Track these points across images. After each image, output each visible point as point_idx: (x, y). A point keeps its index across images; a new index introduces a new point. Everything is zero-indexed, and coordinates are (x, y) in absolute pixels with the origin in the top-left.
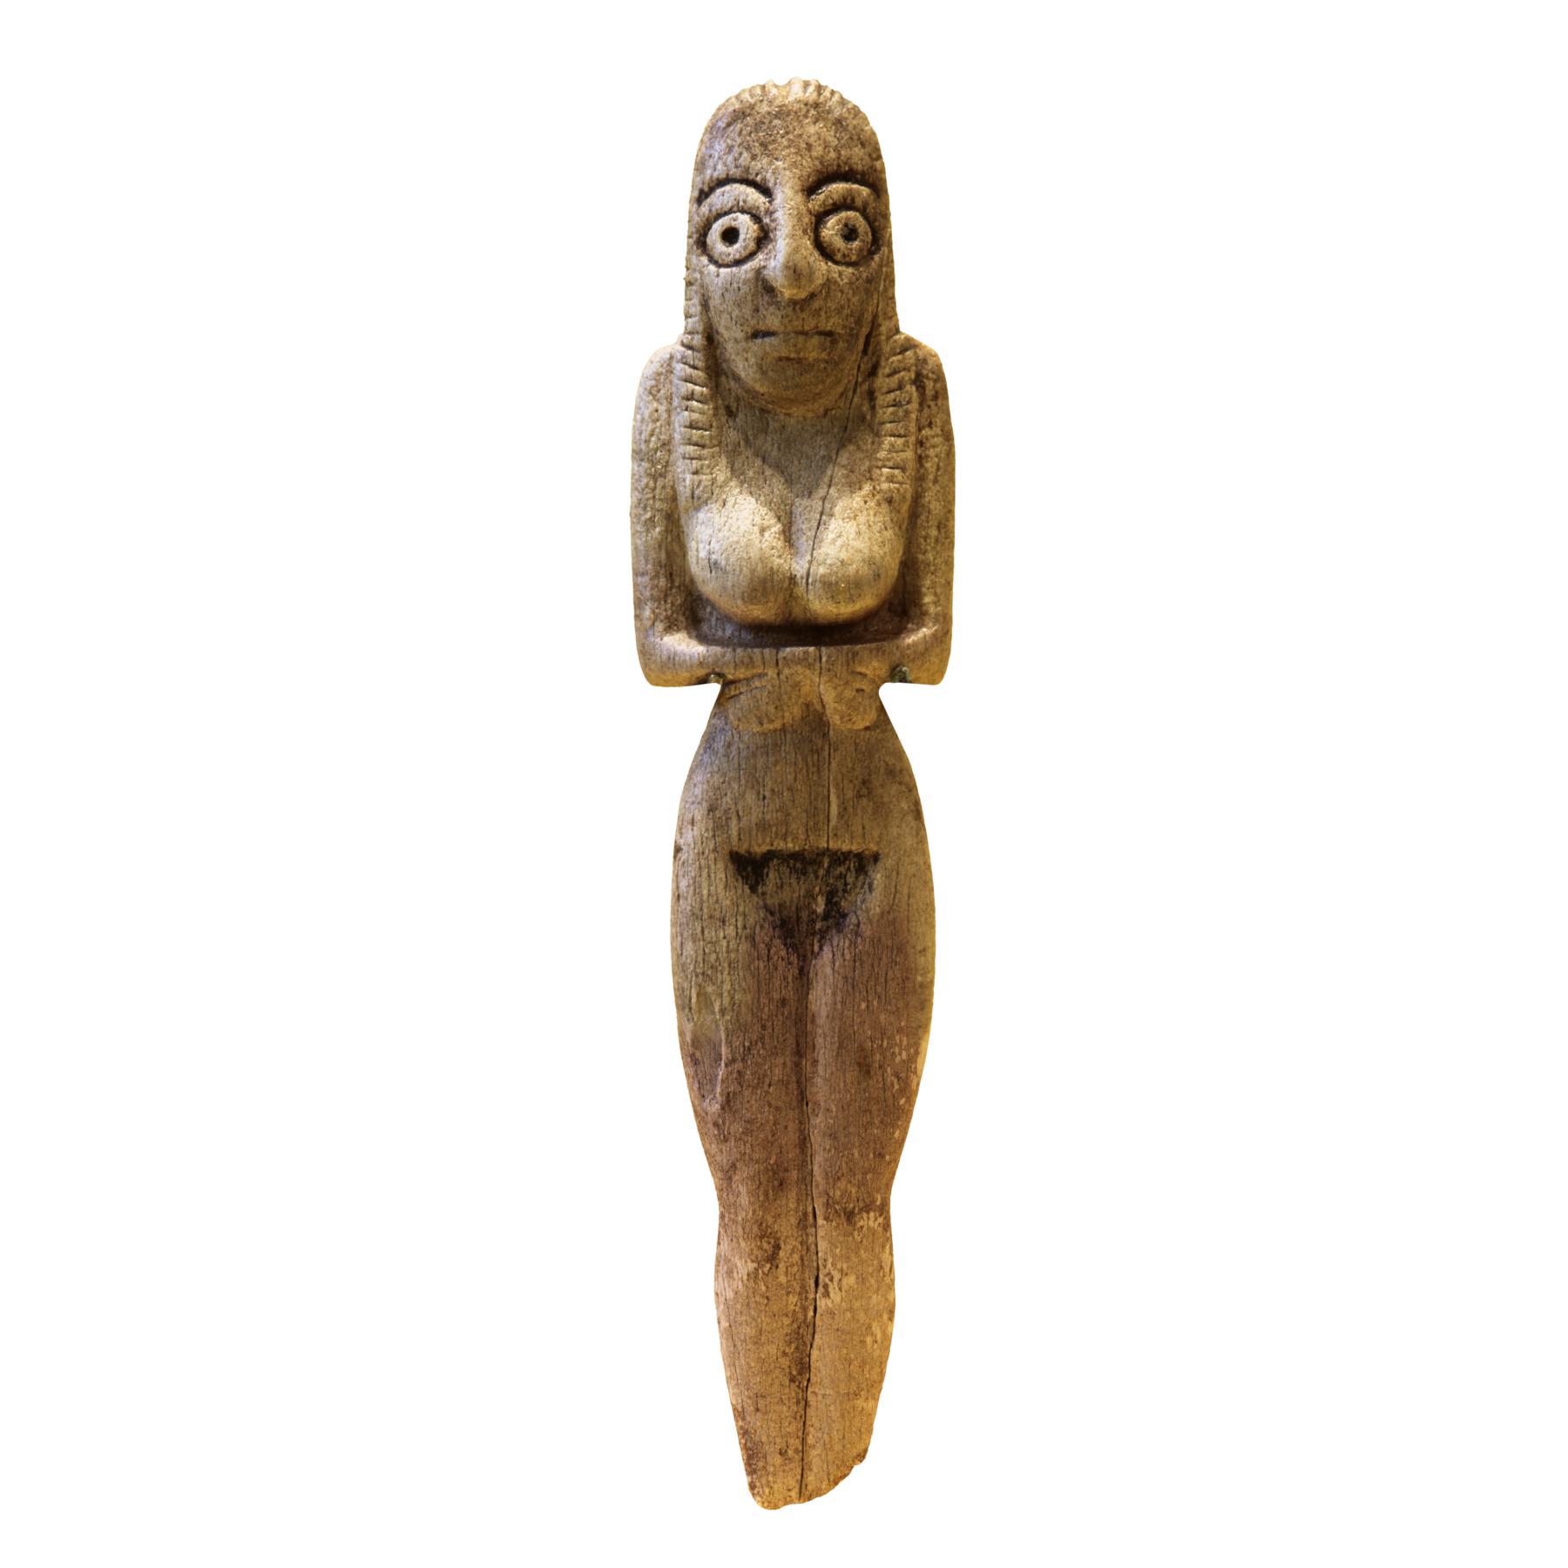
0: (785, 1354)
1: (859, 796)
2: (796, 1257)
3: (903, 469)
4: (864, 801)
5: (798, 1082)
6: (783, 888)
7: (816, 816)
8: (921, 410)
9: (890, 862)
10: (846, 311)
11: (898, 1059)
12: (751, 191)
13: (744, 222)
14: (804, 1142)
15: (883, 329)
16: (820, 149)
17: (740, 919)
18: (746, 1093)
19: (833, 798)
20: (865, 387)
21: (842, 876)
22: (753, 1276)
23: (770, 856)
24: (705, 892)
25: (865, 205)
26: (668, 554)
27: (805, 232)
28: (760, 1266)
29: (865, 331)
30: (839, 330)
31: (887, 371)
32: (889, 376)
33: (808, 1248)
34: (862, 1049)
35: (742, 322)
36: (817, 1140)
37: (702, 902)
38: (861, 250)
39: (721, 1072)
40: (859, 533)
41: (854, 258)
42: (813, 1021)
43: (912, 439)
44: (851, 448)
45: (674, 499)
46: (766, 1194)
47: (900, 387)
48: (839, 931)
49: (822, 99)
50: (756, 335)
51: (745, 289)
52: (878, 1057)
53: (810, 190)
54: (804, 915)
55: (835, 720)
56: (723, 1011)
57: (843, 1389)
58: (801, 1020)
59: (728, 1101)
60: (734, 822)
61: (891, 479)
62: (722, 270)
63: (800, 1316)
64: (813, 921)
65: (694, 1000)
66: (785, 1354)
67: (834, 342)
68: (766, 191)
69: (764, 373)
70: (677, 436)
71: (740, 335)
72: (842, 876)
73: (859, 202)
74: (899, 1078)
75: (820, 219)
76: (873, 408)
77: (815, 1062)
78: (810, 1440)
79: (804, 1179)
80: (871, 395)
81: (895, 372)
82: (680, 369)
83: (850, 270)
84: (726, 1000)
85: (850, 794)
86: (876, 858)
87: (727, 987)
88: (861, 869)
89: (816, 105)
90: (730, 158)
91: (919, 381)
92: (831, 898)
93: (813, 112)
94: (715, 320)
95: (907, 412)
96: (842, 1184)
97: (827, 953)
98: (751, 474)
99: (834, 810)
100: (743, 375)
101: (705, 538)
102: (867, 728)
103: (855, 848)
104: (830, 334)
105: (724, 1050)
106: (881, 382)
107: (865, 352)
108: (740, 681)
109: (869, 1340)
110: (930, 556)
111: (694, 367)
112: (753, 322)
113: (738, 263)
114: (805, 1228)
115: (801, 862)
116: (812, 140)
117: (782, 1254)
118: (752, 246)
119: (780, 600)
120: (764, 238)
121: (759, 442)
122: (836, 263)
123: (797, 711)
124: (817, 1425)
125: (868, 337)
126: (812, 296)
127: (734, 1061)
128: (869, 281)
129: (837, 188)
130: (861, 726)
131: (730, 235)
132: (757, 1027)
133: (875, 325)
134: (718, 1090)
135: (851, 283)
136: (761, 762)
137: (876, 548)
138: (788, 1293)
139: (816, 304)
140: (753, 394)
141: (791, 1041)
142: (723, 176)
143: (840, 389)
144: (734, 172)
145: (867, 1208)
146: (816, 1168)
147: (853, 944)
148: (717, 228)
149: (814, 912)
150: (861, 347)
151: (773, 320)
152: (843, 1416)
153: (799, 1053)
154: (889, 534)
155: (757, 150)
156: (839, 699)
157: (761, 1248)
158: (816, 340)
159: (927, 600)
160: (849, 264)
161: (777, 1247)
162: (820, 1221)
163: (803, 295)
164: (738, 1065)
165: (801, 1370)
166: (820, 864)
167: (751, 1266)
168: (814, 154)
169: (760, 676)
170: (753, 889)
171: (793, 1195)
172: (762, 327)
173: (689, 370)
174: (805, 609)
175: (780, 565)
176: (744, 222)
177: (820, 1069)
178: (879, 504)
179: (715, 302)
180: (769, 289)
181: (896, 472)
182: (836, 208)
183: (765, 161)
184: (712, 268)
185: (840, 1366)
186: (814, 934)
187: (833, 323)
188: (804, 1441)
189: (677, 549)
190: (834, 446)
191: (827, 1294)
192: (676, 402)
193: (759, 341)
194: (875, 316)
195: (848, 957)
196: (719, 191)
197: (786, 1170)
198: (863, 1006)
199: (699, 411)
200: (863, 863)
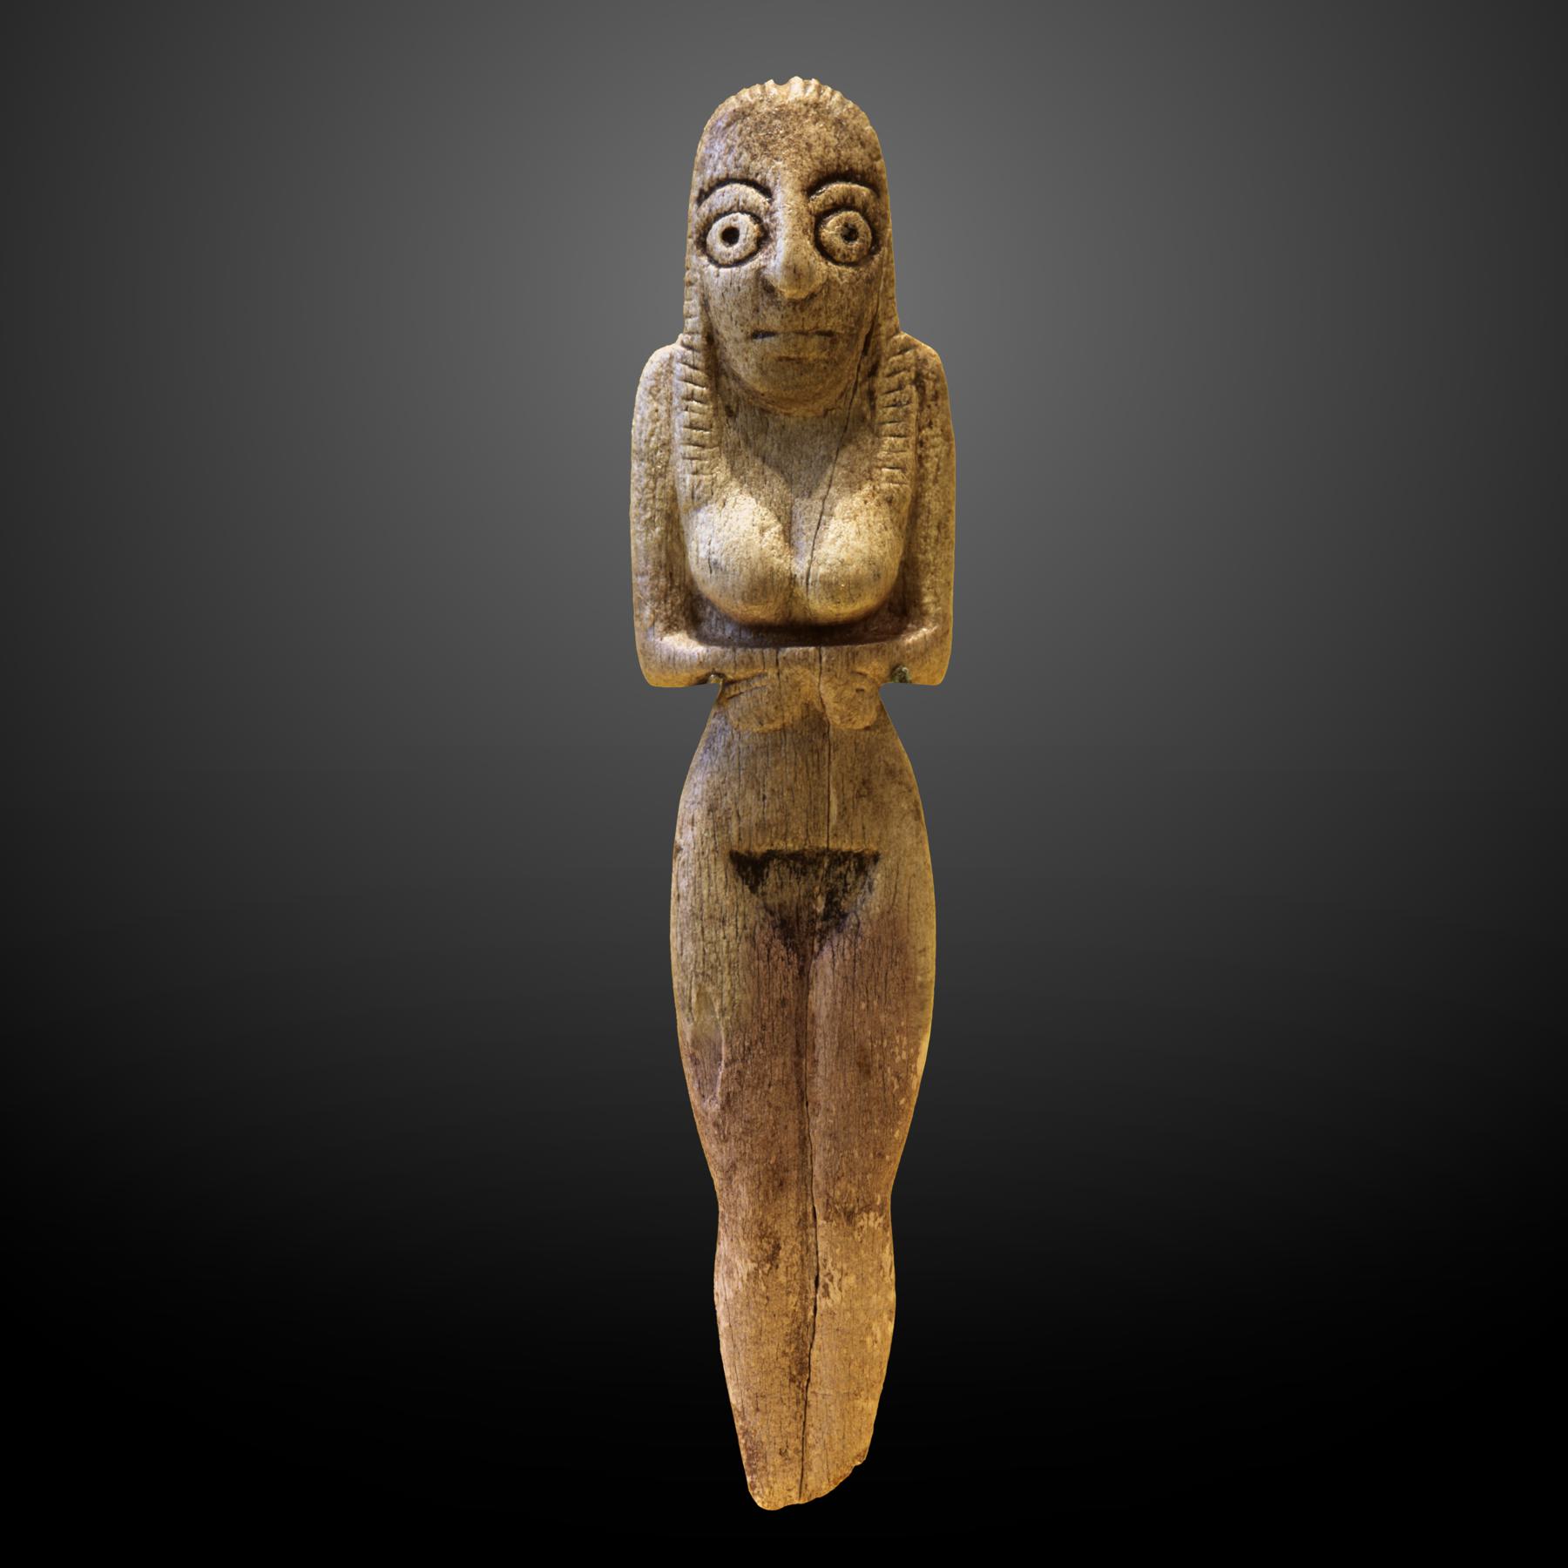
0: (785, 1354)
1: (859, 796)
2: (796, 1257)
3: (903, 469)
4: (864, 801)
5: (798, 1082)
6: (783, 888)
7: (816, 816)
8: (921, 410)
9: (890, 862)
10: (846, 311)
11: (898, 1059)
12: (751, 191)
13: (744, 222)
14: (804, 1142)
15: (883, 329)
16: (820, 149)
17: (740, 919)
18: (746, 1093)
19: (833, 798)
20: (865, 387)
21: (842, 876)
22: (753, 1276)
23: (770, 856)
24: (705, 892)
25: (865, 205)
26: (668, 554)
27: (805, 232)
28: (760, 1266)
29: (865, 331)
30: (839, 330)
31: (887, 371)
32: (889, 376)
33: (808, 1248)
34: (862, 1049)
35: (742, 322)
36: (817, 1140)
37: (702, 902)
38: (861, 250)
39: (721, 1072)
40: (859, 533)
41: (854, 258)
42: (813, 1021)
43: (912, 439)
44: (851, 448)
45: (674, 499)
46: (766, 1194)
47: (900, 387)
48: (839, 931)
49: (822, 99)
50: (756, 335)
51: (745, 289)
52: (878, 1057)
53: (810, 190)
54: (804, 915)
55: (835, 720)
56: (723, 1011)
57: (843, 1389)
58: (801, 1020)
59: (728, 1101)
60: (734, 822)
61: (891, 479)
62: (722, 270)
63: (800, 1316)
64: (813, 921)
65: (694, 1000)
66: (785, 1354)
67: (834, 342)
68: (766, 191)
69: (764, 373)
70: (677, 436)
71: (740, 335)
72: (842, 876)
73: (859, 202)
74: (899, 1078)
75: (820, 219)
76: (873, 408)
77: (815, 1062)
78: (810, 1440)
79: (804, 1179)
80: (871, 395)
81: (895, 372)
82: (680, 369)
83: (850, 270)
84: (726, 1000)
85: (850, 794)
86: (876, 858)
87: (727, 987)
88: (861, 869)
89: (816, 105)
90: (730, 158)
91: (918, 381)
92: (831, 898)
93: (813, 112)
94: (715, 320)
95: (907, 412)
96: (842, 1184)
97: (827, 953)
98: (751, 474)
99: (834, 810)
100: (743, 375)
101: (705, 538)
102: (867, 728)
103: (855, 848)
104: (830, 334)
105: (724, 1050)
106: (881, 382)
107: (865, 352)
108: (740, 681)
109: (869, 1340)
110: (930, 556)
111: (694, 367)
112: (753, 322)
113: (738, 263)
114: (805, 1228)
115: (801, 862)
116: (812, 140)
117: (782, 1254)
118: (752, 246)
119: (780, 600)
120: (764, 238)
121: (759, 442)
122: (836, 263)
123: (797, 711)
124: (817, 1425)
125: (868, 337)
126: (812, 296)
127: (734, 1061)
128: (869, 281)
129: (837, 188)
130: (861, 726)
131: (730, 235)
132: (757, 1027)
133: (875, 325)
134: (718, 1090)
135: (851, 283)
136: (761, 762)
137: (876, 548)
138: (788, 1293)
139: (816, 304)
140: (753, 394)
141: (791, 1041)
142: (723, 176)
143: (840, 389)
144: (734, 172)
145: (867, 1208)
146: (816, 1168)
147: (853, 944)
148: (717, 228)
149: (814, 912)
150: (861, 347)
151: (773, 320)
152: (843, 1416)
153: (799, 1053)
154: (889, 534)
155: (757, 150)
156: (839, 699)
157: (761, 1248)
158: (816, 340)
159: (927, 600)
160: (849, 264)
161: (777, 1247)
162: (820, 1221)
163: (803, 295)
164: (738, 1065)
165: (801, 1370)
166: (820, 864)
167: (751, 1266)
168: (814, 154)
169: (760, 676)
170: (753, 889)
171: (793, 1195)
172: (762, 327)
173: (689, 370)
174: (805, 609)
175: (780, 565)
176: (744, 222)
177: (820, 1069)
178: (879, 504)
179: (715, 302)
180: (769, 289)
181: (896, 472)
182: (836, 208)
183: (765, 161)
184: (712, 268)
185: (840, 1366)
186: (814, 934)
187: (833, 323)
188: (804, 1441)
189: (677, 549)
190: (834, 446)
191: (827, 1294)
192: (676, 402)
193: (759, 341)
194: (875, 316)
195: (848, 957)
196: (719, 191)
197: (786, 1170)
198: (863, 1006)
199: (699, 411)
200: (863, 863)
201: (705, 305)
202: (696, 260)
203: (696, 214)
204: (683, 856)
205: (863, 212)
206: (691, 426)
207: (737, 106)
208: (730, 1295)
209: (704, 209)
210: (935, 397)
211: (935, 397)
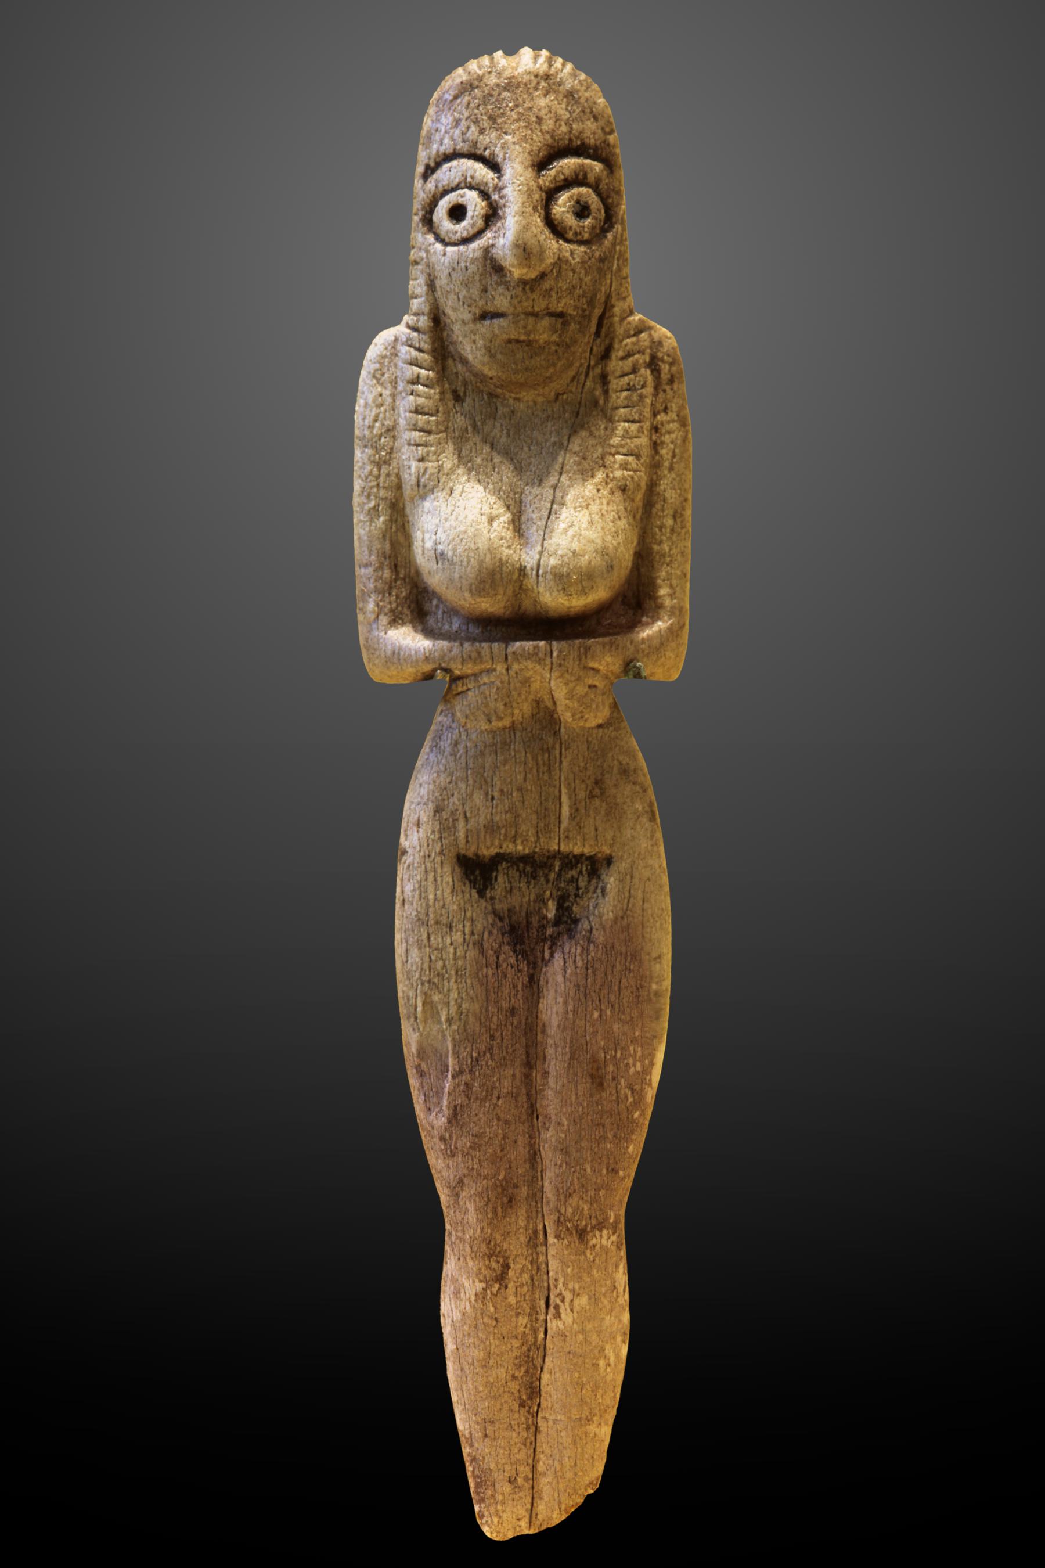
0: (514, 1377)
1: (592, 796)
2: (526, 1277)
3: (638, 456)
4: (597, 802)
6: (512, 892)
7: (547, 817)
8: (656, 395)
9: (622, 864)
10: (578, 292)
11: (632, 1070)
13: (471, 199)
14: (534, 1156)
15: (617, 310)
16: (551, 122)
17: (468, 924)
18: (474, 1106)
19: (565, 799)
21: (574, 880)
22: (481, 1296)
23: (498, 859)
24: (431, 897)
25: (598, 181)
27: (535, 209)
28: (489, 1286)
29: (597, 312)
31: (621, 354)
32: (623, 358)
33: (539, 1269)
34: (594, 1060)
35: (469, 303)
36: (548, 1155)
37: (428, 906)
38: (593, 228)
40: (591, 523)
41: (586, 236)
42: (544, 1032)
43: (647, 425)
44: (584, 433)
45: (399, 487)
47: (634, 370)
49: (553, 71)
50: (484, 316)
52: (611, 1068)
53: (541, 165)
54: (534, 920)
55: (567, 717)
58: (531, 1030)
60: (461, 824)
61: (624, 466)
62: (449, 249)
63: (531, 1339)
64: (544, 927)
65: (419, 1009)
66: (514, 1377)
67: (565, 324)
68: (495, 167)
69: (492, 356)
70: (402, 422)
71: (467, 316)
72: (574, 880)
73: (591, 178)
74: (633, 1091)
75: (550, 195)
76: (606, 392)
77: (546, 1074)
78: (541, 1467)
80: (604, 379)
81: (629, 355)
82: (404, 350)
83: (583, 248)
84: (453, 1010)
85: (582, 795)
86: (609, 861)
87: (454, 995)
89: (547, 77)
93: (543, 84)
94: (442, 301)
95: (641, 397)
96: (574, 1201)
97: (558, 960)
98: (479, 461)
99: (566, 811)
100: (470, 358)
102: (600, 726)
103: (587, 851)
104: (561, 315)
106: (615, 365)
107: (598, 333)
109: (602, 1363)
110: (666, 547)
111: (420, 350)
112: (481, 303)
113: (466, 241)
114: (535, 1246)
115: (532, 865)
116: (542, 113)
117: (511, 1273)
118: (480, 223)
119: (510, 592)
120: (492, 216)
122: (568, 241)
124: (548, 1451)
125: (601, 319)
126: (543, 275)
128: (602, 260)
129: (569, 163)
131: (457, 213)
132: (485, 1037)
133: (608, 306)
134: (445, 1102)
135: (583, 262)
136: (489, 761)
137: (609, 538)
138: (518, 1315)
139: (547, 285)
140: (481, 378)
141: (521, 1051)
142: (450, 151)
146: (546, 1184)
147: (585, 950)
149: (545, 917)
150: (593, 329)
151: (501, 301)
152: (574, 1442)
153: (529, 1064)
154: (622, 524)
157: (489, 1267)
158: (546, 322)
160: (581, 243)
161: (506, 1267)
162: (551, 1240)
163: (533, 275)
164: (466, 1077)
166: (551, 867)
167: (480, 1286)
168: (545, 127)
169: (489, 671)
170: (481, 894)
171: (522, 1212)
172: (490, 308)
173: (414, 353)
174: (535, 602)
176: (471, 199)
178: (612, 493)
179: (441, 282)
180: (498, 269)
181: (630, 459)
182: (567, 184)
183: (494, 135)
184: (439, 246)
186: (544, 940)
189: (401, 539)
190: (566, 432)
191: (558, 1316)
193: (487, 322)
194: (608, 297)
195: (580, 964)
197: (516, 1186)
198: (596, 1015)
199: (425, 395)
201: (431, 285)
202: (422, 238)
203: (422, 190)
204: (408, 859)
205: (596, 189)
206: (417, 411)
207: (465, 78)
208: (457, 1316)
209: (431, 185)
210: (671, 381)
211: (671, 381)
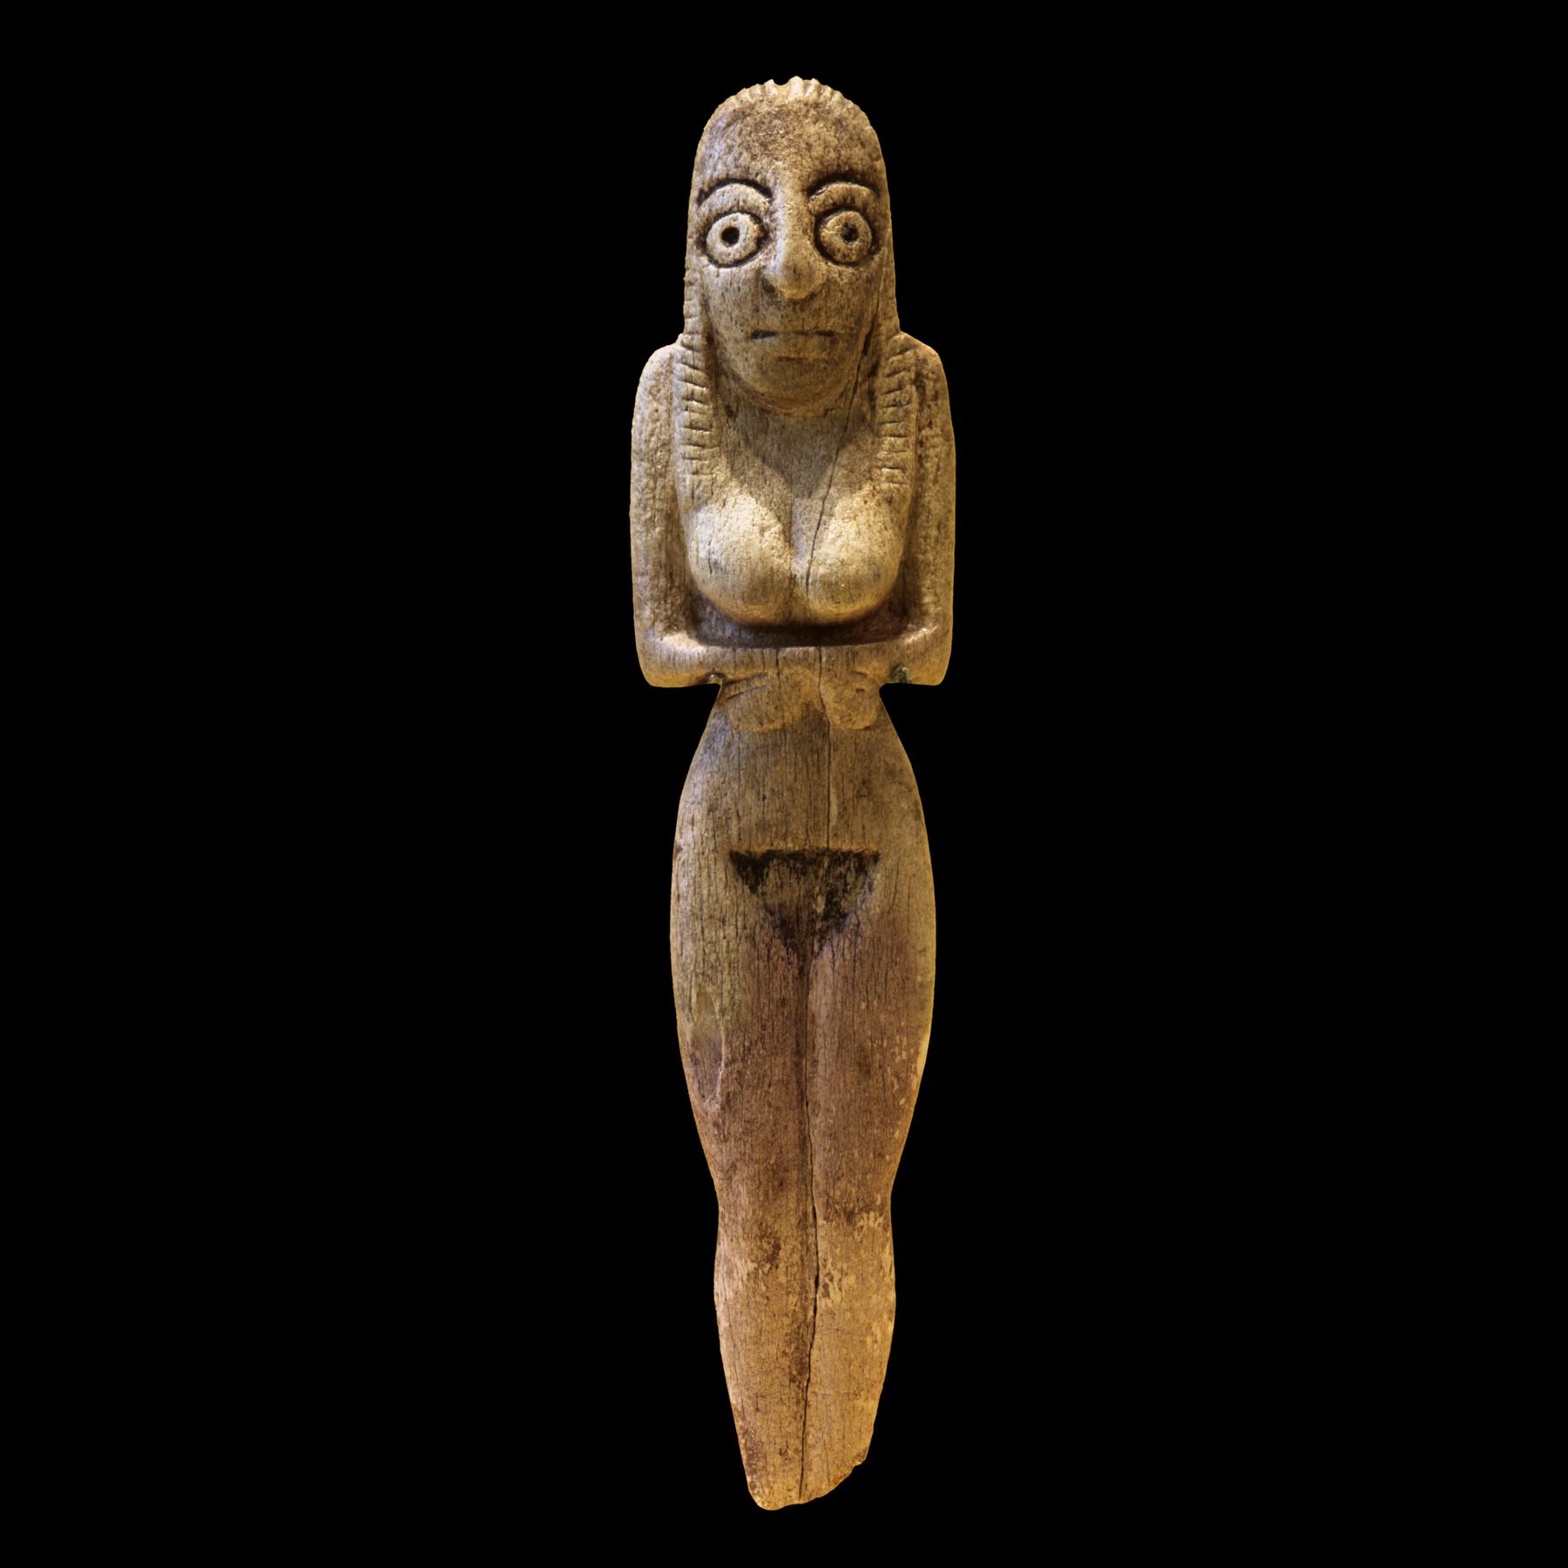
0: (785, 1354)
1: (859, 796)
2: (796, 1257)
3: (903, 469)
4: (864, 801)
5: (798, 1082)
6: (783, 888)
8: (921, 410)
9: (890, 862)
10: (846, 311)
11: (898, 1059)
12: (751, 191)
13: (744, 222)
14: (804, 1142)
15: (883, 329)
16: (820, 149)
17: (740, 919)
18: (746, 1093)
19: (833, 798)
20: (865, 387)
21: (842, 876)
22: (753, 1276)
23: (770, 856)
24: (705, 892)
25: (865, 205)
26: (668, 554)
27: (805, 232)
28: (760, 1266)
29: (865, 331)
30: (839, 330)
31: (887, 371)
32: (889, 376)
33: (808, 1248)
34: (862, 1049)
35: (742, 322)
36: (817, 1140)
37: (702, 902)
38: (861, 250)
39: (721, 1072)
40: (859, 533)
41: (854, 258)
42: (813, 1021)
43: (912, 439)
44: (851, 448)
45: (674, 499)
46: (766, 1194)
47: (900, 387)
48: (839, 931)
49: (822, 99)
50: (756, 335)
51: (745, 289)
52: (878, 1057)
53: (810, 190)
54: (804, 915)
55: (835, 720)
56: (723, 1011)
57: (843, 1389)
58: (801, 1020)
59: (728, 1101)
60: (734, 822)
61: (891, 479)
62: (722, 270)
63: (800, 1316)
64: (813, 921)
65: (694, 1000)
66: (785, 1354)
67: (834, 342)
68: (766, 191)
69: (764, 373)
70: (677, 436)
71: (740, 335)
72: (842, 876)
73: (859, 202)
74: (899, 1078)
75: (820, 219)
76: (873, 408)
77: (815, 1062)
78: (810, 1440)
79: (804, 1179)
80: (871, 395)
81: (895, 372)
83: (850, 270)
84: (726, 1000)
85: (850, 794)
86: (876, 858)
87: (727, 987)
88: (861, 869)
89: (816, 105)
90: (730, 158)
92: (831, 898)
93: (813, 112)
94: (715, 320)
95: (907, 412)
96: (842, 1184)
97: (827, 953)
98: (751, 474)
99: (834, 810)
100: (743, 375)
101: (705, 538)
102: (867, 728)
103: (855, 848)
104: (830, 334)
105: (724, 1050)
106: (881, 382)
107: (865, 352)
108: (740, 681)
109: (869, 1340)
110: (930, 556)
111: (694, 367)
112: (753, 322)
113: (738, 263)
114: (805, 1228)
115: (801, 862)
116: (812, 140)
117: (782, 1254)
118: (752, 246)
119: (780, 600)
120: (764, 238)
121: (759, 442)
122: (836, 263)
123: (797, 711)
124: (817, 1425)
125: (868, 337)
126: (812, 296)
127: (734, 1061)
128: (869, 281)
129: (837, 188)
130: (861, 726)
131: (730, 235)
132: (757, 1027)
134: (718, 1090)
135: (851, 283)
136: (761, 762)
137: (876, 548)
138: (788, 1293)
139: (816, 304)
140: (753, 394)
141: (791, 1041)
142: (723, 176)
143: (840, 389)
144: (734, 172)
146: (816, 1168)
147: (853, 944)
148: (717, 228)
149: (814, 912)
150: (861, 347)
151: (773, 320)
152: (843, 1416)
153: (799, 1053)
154: (889, 534)
155: (757, 150)
156: (839, 699)
157: (761, 1248)
158: (816, 340)
159: (927, 600)
160: (849, 264)
161: (777, 1247)
162: (820, 1221)
163: (803, 295)
164: (738, 1065)
165: (801, 1370)
166: (820, 864)
167: (751, 1266)
168: (814, 154)
169: (760, 676)
170: (753, 889)
171: (793, 1195)
172: (762, 327)
173: (689, 370)
174: (805, 609)
175: (780, 565)
176: (744, 222)
177: (820, 1069)
178: (879, 504)
179: (715, 302)
180: (769, 289)
181: (896, 472)
182: (836, 208)
183: (765, 161)
184: (712, 268)
185: (840, 1366)
186: (814, 934)
187: (833, 323)
188: (804, 1441)
189: (677, 549)
190: (834, 446)
191: (827, 1294)
192: (676, 402)
193: (759, 341)
194: (875, 316)
195: (848, 957)
196: (719, 191)
197: (786, 1170)
198: (863, 1006)
199: (699, 411)
200: (863, 863)
206: (691, 426)
207: (737, 106)
208: (730, 1295)
209: (704, 209)
